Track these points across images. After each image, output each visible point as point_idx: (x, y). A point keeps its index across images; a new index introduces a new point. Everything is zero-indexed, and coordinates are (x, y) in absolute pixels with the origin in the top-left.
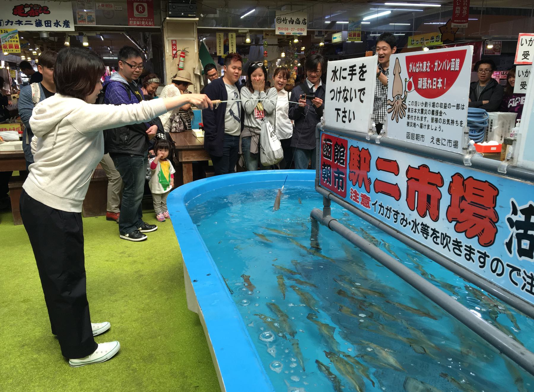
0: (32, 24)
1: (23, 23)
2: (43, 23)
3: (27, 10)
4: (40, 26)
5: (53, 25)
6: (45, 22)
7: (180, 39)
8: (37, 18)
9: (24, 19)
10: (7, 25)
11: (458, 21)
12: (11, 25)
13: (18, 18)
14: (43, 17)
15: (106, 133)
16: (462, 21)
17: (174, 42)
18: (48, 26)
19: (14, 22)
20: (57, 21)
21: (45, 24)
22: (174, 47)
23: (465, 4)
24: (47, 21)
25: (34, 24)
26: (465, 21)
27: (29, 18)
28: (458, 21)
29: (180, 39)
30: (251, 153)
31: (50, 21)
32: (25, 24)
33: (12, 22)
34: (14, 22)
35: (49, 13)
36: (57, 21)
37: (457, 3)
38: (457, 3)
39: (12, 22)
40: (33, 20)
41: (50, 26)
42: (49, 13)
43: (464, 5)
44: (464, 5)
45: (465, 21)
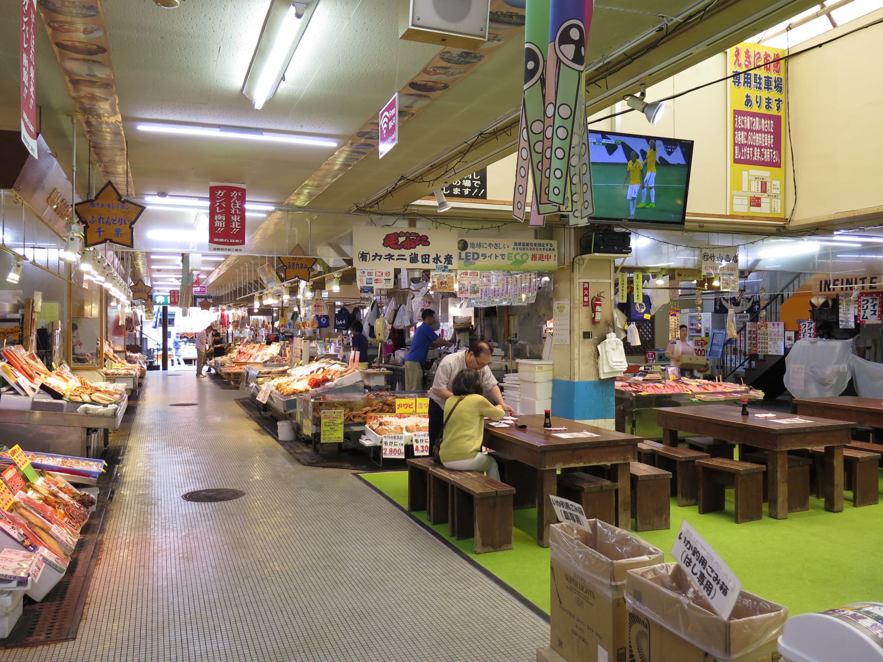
0: (406, 259)
1: (395, 257)
2: (420, 258)
3: (401, 239)
4: (415, 262)
5: (431, 260)
6: (422, 256)
7: (594, 281)
8: (412, 251)
9: (396, 253)
10: (373, 260)
11: (222, 240)
12: (380, 260)
13: (389, 250)
14: (420, 250)
15: (798, 421)
16: (232, 241)
17: (586, 285)
18: (425, 262)
19: (384, 256)
20: (437, 255)
21: (422, 259)
22: (586, 292)
23: (235, 212)
24: (425, 255)
25: (409, 260)
26: (237, 241)
27: (403, 251)
28: (222, 240)
29: (594, 281)
30: (631, 474)
31: (429, 256)
32: (397, 259)
33: (381, 256)
34: (384, 256)
35: (428, 244)
36: (437, 255)
37: (218, 208)
38: (218, 208)
39: (381, 256)
40: (407, 253)
41: (428, 262)
42: (428, 244)
43: (233, 212)
44: (233, 212)
45: (237, 241)
